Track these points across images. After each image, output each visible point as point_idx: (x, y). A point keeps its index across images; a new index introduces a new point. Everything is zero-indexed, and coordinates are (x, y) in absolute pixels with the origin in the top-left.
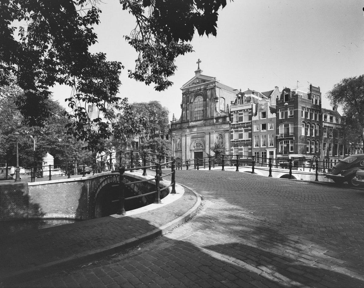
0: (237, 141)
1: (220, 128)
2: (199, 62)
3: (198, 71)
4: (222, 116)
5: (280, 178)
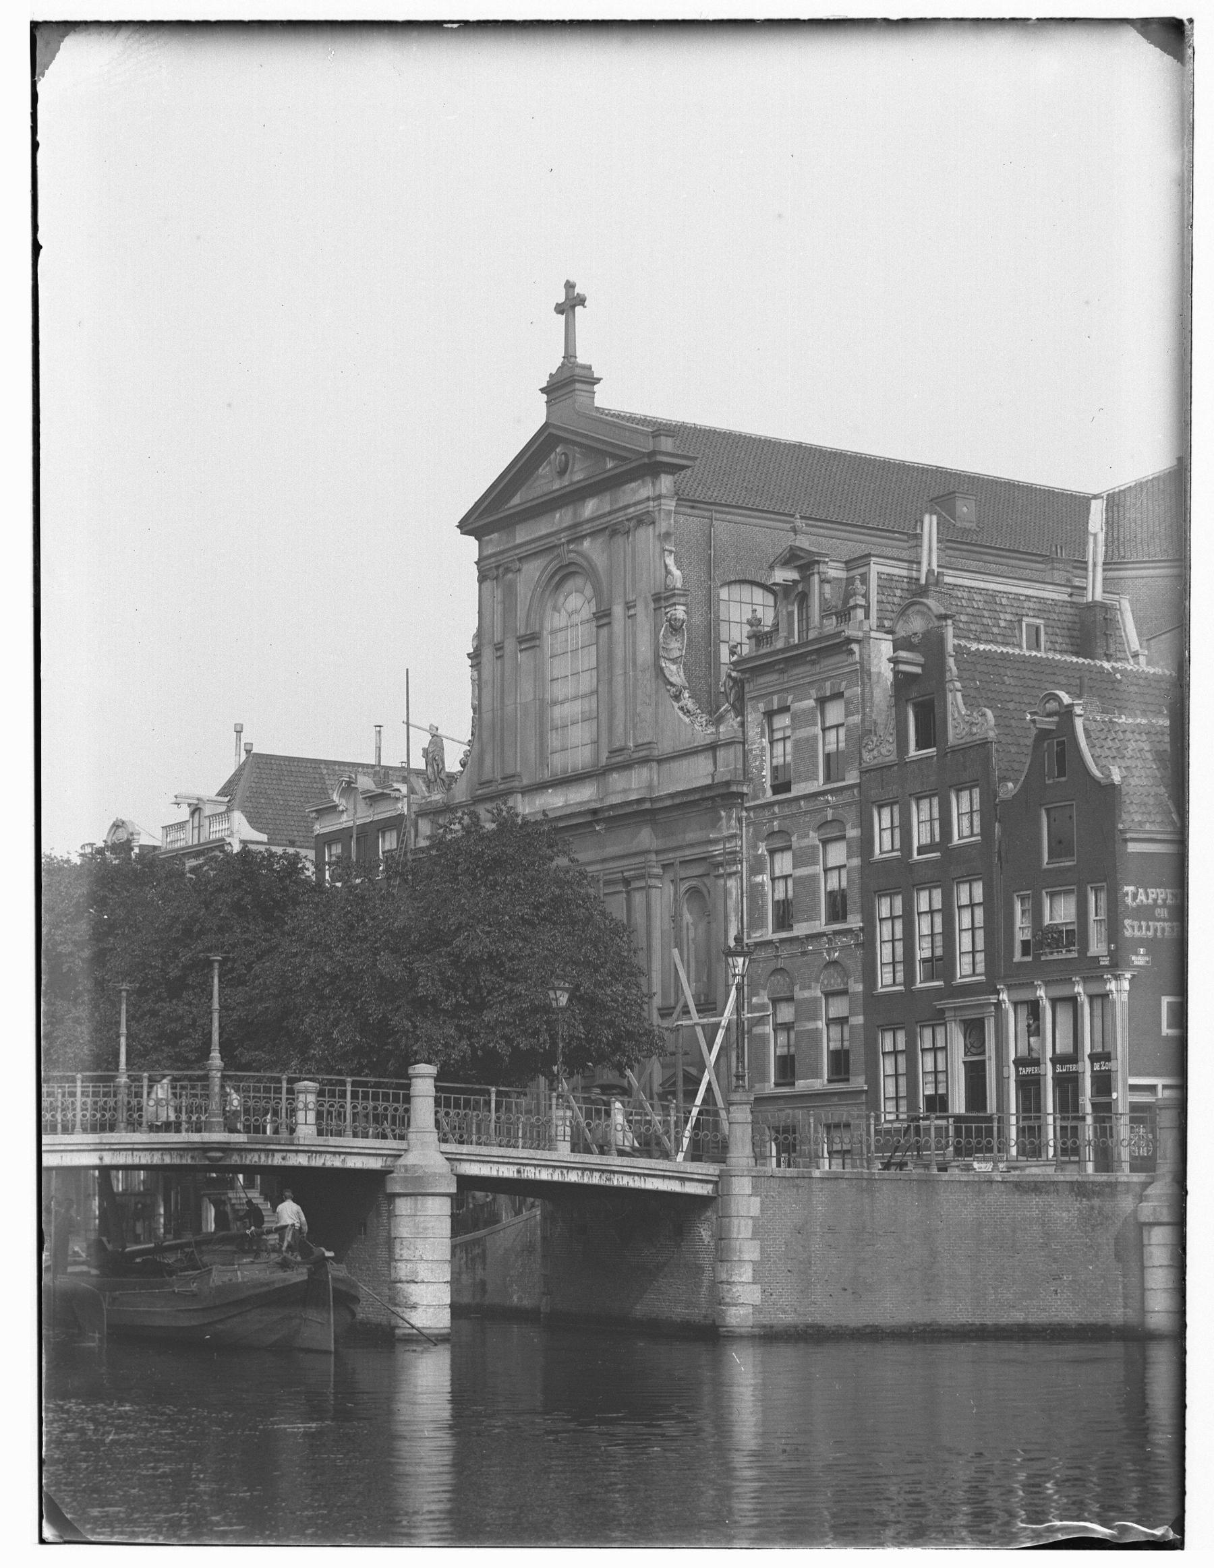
2: (571, 304)
3: (569, 383)
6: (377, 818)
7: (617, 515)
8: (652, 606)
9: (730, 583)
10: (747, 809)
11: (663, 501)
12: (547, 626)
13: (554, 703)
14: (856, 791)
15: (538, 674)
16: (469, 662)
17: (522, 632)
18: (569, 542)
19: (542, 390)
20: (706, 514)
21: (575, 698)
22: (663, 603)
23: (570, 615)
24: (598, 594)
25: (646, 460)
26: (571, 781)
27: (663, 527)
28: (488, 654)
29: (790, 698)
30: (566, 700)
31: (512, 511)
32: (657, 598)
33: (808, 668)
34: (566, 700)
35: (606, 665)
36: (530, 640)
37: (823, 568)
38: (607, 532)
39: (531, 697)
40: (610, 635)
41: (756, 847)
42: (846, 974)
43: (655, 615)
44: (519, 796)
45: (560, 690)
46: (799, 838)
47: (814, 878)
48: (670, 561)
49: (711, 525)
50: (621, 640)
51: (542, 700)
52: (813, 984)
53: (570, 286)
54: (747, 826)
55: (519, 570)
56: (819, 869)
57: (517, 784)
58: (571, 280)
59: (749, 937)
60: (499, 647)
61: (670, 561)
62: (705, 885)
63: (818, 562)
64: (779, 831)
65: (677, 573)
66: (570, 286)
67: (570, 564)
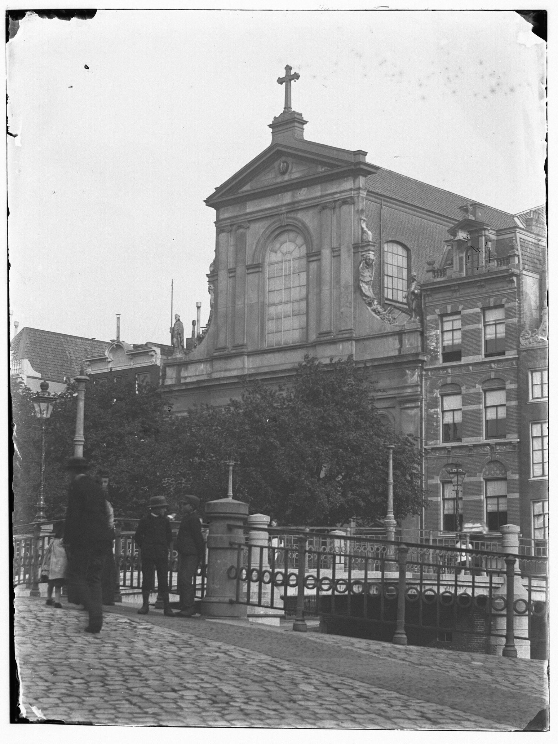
2: (289, 78)
3: (288, 122)
6: (135, 366)
7: (328, 198)
8: (352, 250)
10: (426, 370)
11: (361, 191)
12: (267, 260)
13: (271, 305)
14: (514, 363)
15: (261, 289)
16: (207, 279)
17: (249, 263)
18: (287, 212)
19: (270, 126)
20: (379, 201)
21: (287, 302)
22: (360, 250)
23: (284, 255)
24: (308, 241)
25: (353, 167)
26: (288, 350)
27: (361, 205)
28: (223, 275)
29: (461, 307)
30: (281, 303)
31: (241, 195)
32: (356, 247)
33: (476, 289)
34: (281, 303)
35: (315, 283)
36: (257, 267)
37: (487, 233)
38: (319, 207)
39: (256, 300)
40: (319, 269)
41: (432, 392)
42: (505, 468)
43: (354, 256)
44: (246, 357)
45: (274, 298)
46: (467, 388)
47: (479, 411)
48: (364, 226)
49: (381, 208)
50: (329, 268)
51: (263, 303)
52: (478, 474)
53: (288, 68)
54: (426, 379)
55: (248, 228)
56: (482, 406)
57: (245, 350)
58: (290, 65)
59: (426, 445)
60: (232, 271)
61: (364, 226)
62: (391, 413)
63: (485, 229)
64: (452, 384)
65: (370, 233)
66: (288, 68)
67: (287, 225)
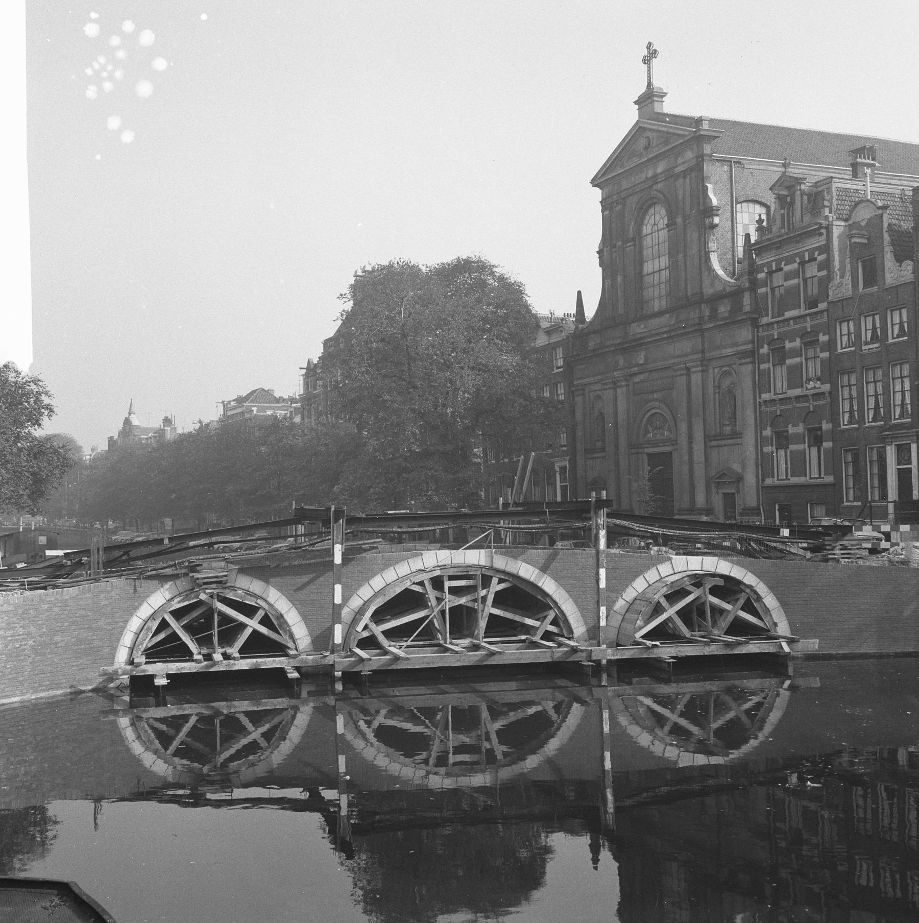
0: (780, 400)
1: (723, 343)
2: (651, 55)
3: (648, 99)
4: (728, 289)
5: (418, 709)
9: (741, 202)
19: (636, 103)
